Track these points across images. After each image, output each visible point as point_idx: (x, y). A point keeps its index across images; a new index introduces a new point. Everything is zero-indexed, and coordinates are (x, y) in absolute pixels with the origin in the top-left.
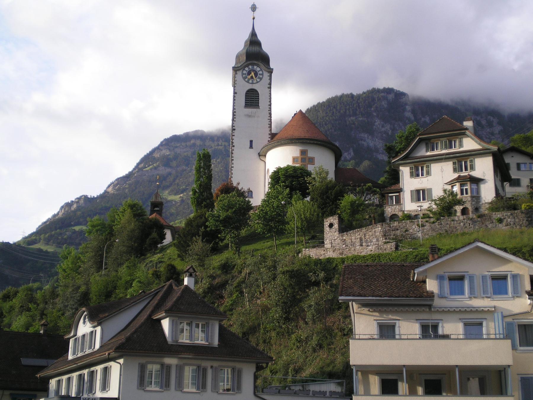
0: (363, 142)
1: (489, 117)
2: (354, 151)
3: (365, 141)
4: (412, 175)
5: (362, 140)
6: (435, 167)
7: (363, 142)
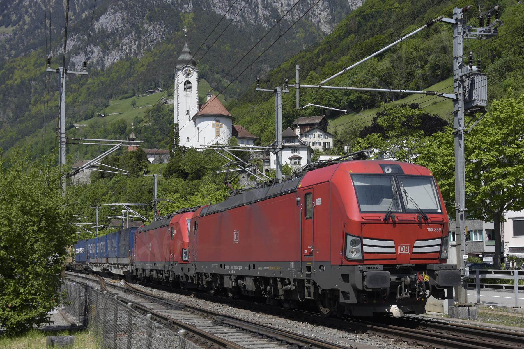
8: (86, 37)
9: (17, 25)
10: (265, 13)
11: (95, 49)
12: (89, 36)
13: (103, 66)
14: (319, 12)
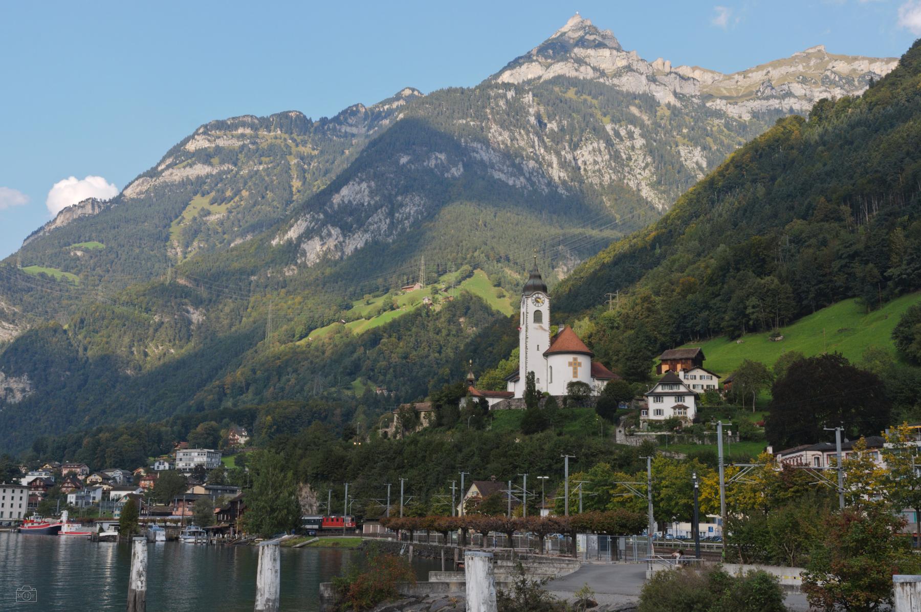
0: (475, 155)
1: (629, 126)
2: (464, 166)
3: (477, 152)
4: (654, 401)
5: (474, 151)
6: (666, 399)
7: (475, 155)
8: (322, 216)
9: (232, 202)
10: (562, 175)
11: (333, 232)
12: (325, 213)
13: (343, 253)
14: (639, 171)
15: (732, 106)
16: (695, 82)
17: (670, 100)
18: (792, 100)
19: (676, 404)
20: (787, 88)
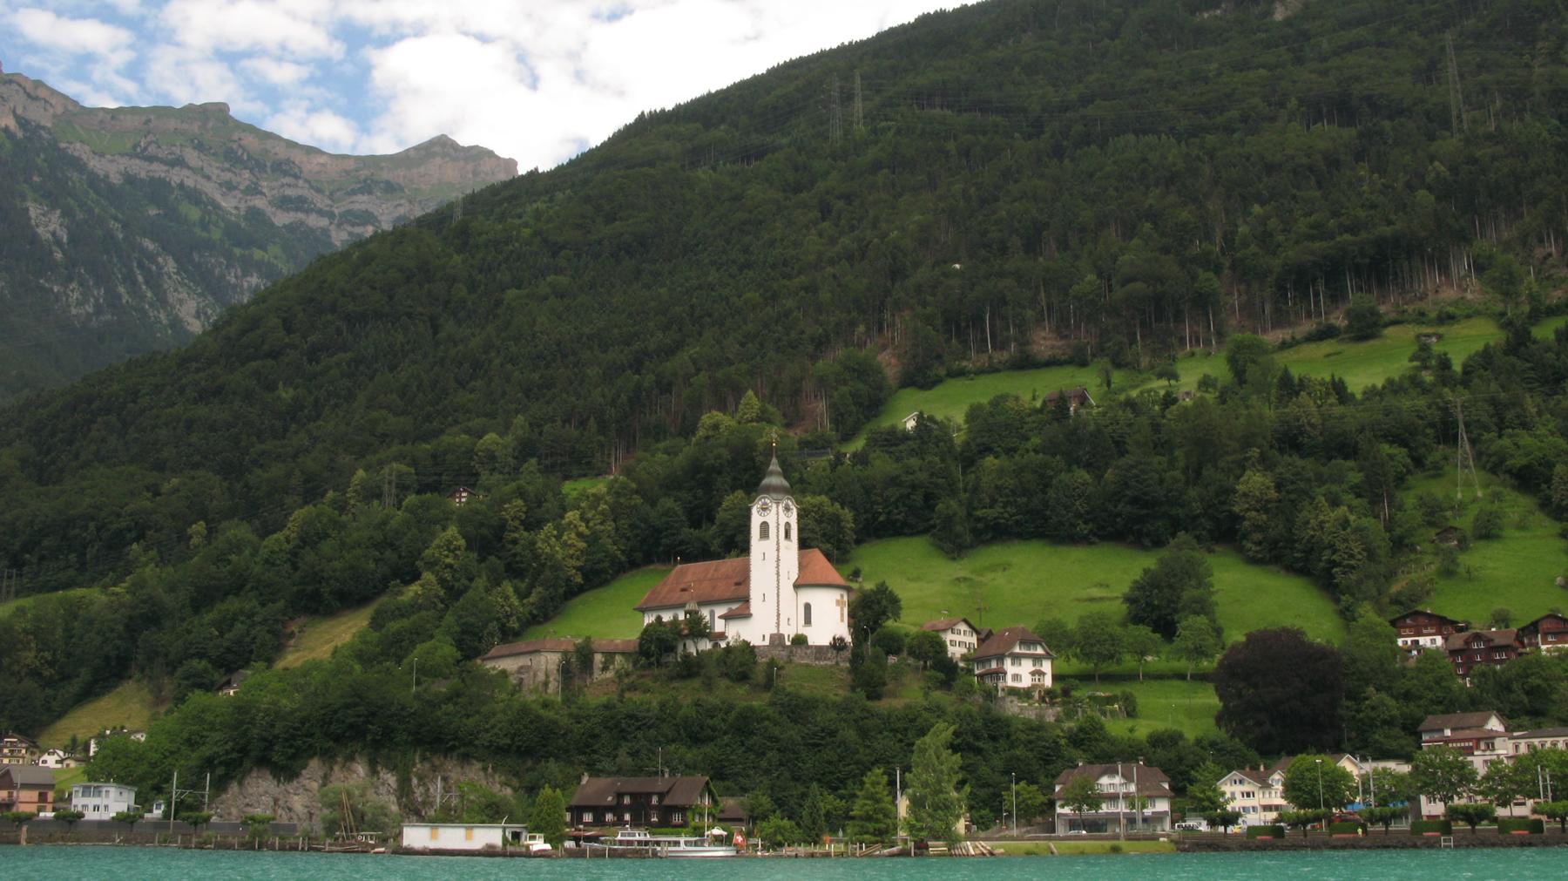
15: (97, 158)
16: (48, 107)
17: (8, 124)
18: (186, 172)
19: (1033, 669)
20: (178, 152)
